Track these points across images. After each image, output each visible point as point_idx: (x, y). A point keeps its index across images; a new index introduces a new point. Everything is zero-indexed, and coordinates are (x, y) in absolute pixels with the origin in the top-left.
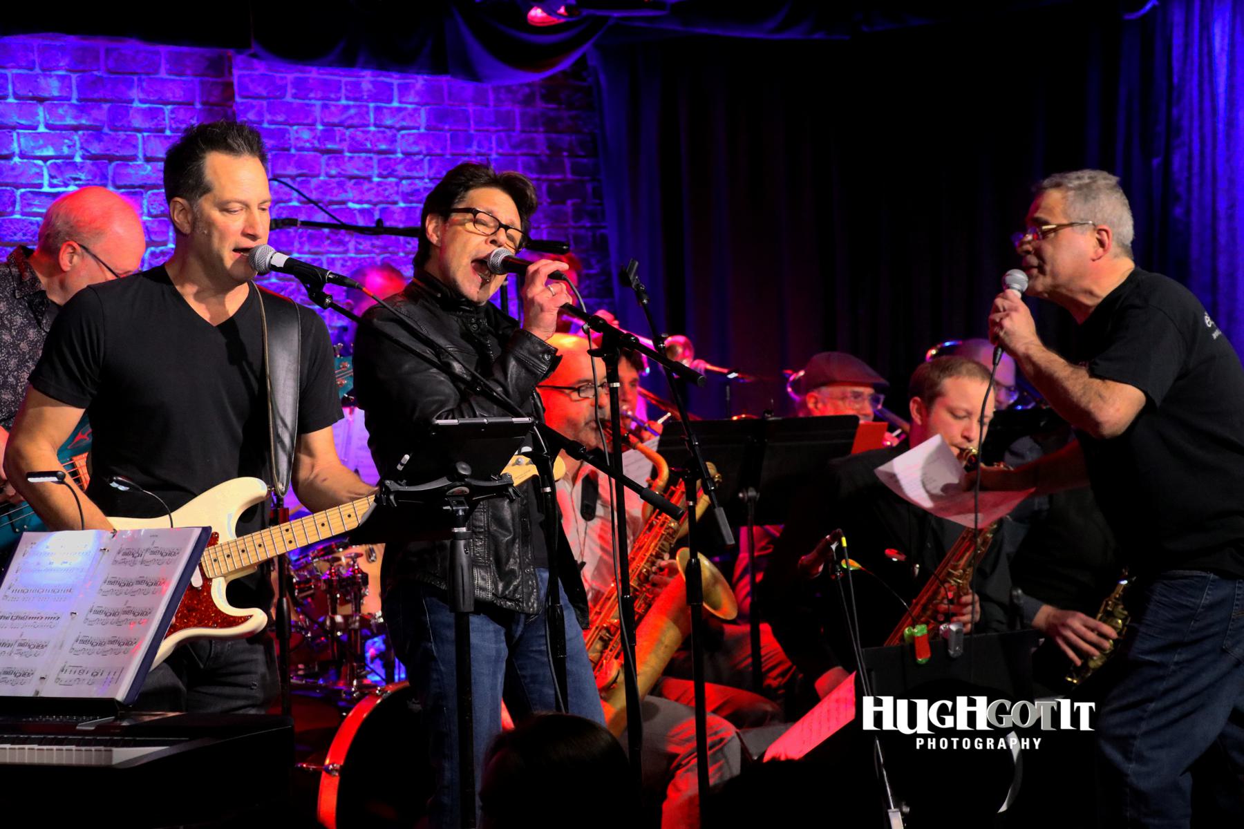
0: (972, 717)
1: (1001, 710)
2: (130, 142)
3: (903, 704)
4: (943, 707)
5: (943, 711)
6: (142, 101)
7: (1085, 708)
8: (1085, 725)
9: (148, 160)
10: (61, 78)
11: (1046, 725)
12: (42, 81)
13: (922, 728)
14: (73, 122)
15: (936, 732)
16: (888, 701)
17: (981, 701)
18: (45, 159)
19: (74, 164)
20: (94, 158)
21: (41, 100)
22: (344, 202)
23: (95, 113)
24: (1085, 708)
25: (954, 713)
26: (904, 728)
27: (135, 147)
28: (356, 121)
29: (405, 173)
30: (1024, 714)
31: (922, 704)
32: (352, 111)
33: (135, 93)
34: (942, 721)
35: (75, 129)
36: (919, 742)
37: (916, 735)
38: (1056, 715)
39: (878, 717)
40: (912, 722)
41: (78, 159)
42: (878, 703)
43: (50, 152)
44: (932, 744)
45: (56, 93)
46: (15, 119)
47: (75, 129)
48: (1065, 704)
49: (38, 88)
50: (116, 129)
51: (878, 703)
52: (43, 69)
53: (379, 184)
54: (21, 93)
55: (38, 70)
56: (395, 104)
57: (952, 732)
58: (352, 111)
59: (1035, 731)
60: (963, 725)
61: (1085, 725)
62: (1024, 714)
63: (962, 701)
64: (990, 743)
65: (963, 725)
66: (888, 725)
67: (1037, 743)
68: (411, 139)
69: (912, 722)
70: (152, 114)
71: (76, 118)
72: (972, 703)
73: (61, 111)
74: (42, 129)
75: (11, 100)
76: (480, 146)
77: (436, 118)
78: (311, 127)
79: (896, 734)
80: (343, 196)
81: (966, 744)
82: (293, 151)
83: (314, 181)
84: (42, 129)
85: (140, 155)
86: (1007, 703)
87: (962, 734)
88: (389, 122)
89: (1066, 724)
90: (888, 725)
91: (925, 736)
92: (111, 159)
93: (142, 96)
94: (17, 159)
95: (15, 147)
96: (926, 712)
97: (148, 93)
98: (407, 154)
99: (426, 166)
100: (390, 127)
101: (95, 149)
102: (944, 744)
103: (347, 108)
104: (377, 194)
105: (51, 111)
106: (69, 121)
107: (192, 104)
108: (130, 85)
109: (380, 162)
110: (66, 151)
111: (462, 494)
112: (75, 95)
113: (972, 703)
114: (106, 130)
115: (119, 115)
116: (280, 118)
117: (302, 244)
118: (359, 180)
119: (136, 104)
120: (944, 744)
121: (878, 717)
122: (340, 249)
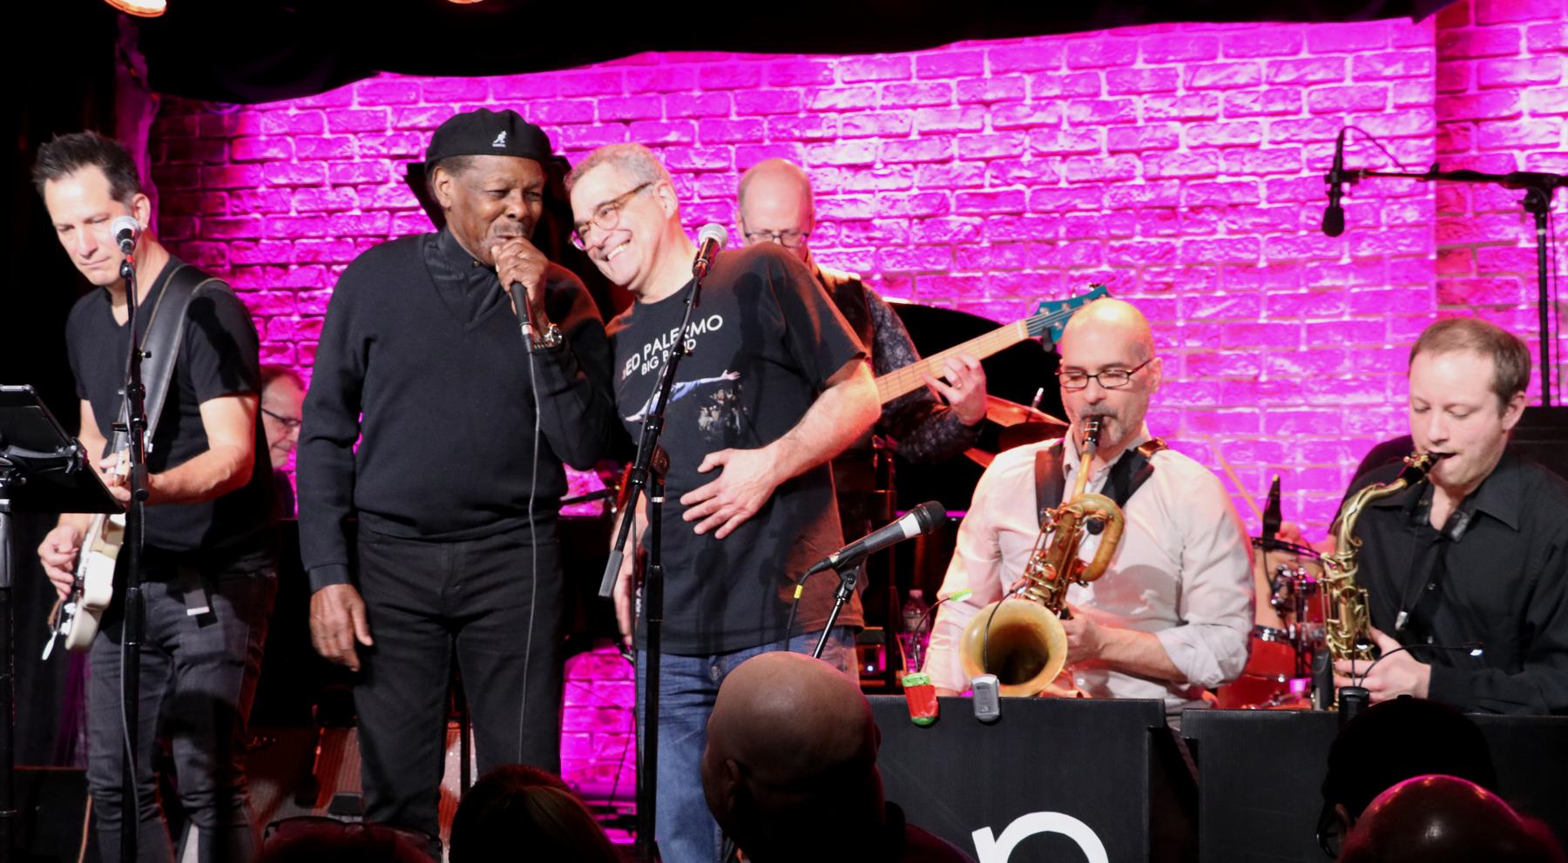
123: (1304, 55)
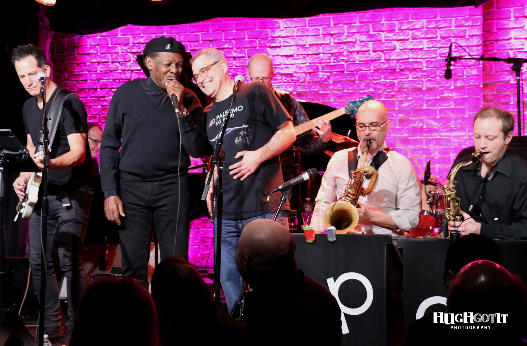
0: (468, 319)
1: (478, 317)
3: (446, 315)
5: (459, 317)
7: (505, 316)
8: (505, 322)
11: (492, 322)
13: (452, 322)
15: (457, 324)
17: (471, 314)
24: (505, 316)
25: (463, 318)
26: (446, 322)
30: (485, 318)
31: (452, 315)
34: (459, 320)
36: (452, 327)
37: (450, 325)
38: (495, 319)
39: (438, 319)
40: (449, 321)
42: (438, 314)
44: (455, 328)
48: (498, 315)
51: (438, 314)
57: (462, 324)
59: (489, 323)
60: (465, 321)
61: (505, 322)
62: (485, 318)
63: (465, 314)
64: (474, 327)
65: (465, 321)
66: (441, 321)
69: (449, 321)
72: (468, 314)
86: (480, 315)
87: (465, 324)
89: (499, 321)
90: (441, 321)
91: (453, 325)
94: (513, 40)
113: (468, 314)
121: (438, 319)
123: (438, 18)
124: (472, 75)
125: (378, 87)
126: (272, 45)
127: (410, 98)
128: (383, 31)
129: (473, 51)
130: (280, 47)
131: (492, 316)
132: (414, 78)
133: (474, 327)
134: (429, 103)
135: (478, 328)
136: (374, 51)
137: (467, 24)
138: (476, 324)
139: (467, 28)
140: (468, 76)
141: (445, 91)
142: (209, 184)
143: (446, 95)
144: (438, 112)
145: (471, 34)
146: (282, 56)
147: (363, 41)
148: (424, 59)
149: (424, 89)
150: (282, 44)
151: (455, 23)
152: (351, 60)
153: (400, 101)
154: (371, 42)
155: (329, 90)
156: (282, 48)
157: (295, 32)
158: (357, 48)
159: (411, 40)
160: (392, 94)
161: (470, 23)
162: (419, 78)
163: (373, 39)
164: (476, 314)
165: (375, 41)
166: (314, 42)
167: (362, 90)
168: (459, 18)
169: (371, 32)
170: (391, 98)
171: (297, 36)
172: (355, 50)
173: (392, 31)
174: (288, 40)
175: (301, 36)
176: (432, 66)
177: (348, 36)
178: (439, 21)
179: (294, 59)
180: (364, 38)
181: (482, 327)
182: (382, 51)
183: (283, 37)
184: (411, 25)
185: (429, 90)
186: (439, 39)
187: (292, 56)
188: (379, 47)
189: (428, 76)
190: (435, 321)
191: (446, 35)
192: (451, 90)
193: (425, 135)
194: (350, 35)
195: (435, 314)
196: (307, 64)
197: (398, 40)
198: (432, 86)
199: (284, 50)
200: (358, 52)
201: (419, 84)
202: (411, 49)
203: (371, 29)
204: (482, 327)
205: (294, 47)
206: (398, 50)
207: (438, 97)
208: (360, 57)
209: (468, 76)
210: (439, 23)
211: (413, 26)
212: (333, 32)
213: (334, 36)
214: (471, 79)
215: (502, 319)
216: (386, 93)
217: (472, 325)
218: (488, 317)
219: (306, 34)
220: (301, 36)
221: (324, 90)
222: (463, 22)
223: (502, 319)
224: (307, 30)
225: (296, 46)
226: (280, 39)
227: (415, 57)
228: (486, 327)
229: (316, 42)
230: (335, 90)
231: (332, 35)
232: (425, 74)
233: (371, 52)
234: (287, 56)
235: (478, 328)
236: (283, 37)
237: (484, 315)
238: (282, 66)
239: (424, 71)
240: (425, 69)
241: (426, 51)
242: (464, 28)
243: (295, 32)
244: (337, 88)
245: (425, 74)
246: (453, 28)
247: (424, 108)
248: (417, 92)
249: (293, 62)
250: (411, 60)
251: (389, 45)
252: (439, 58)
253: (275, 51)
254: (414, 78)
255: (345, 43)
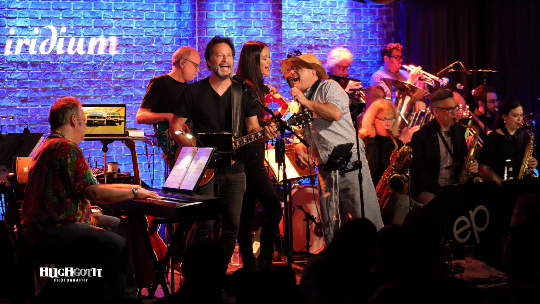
0: (69, 273)
1: (77, 271)
2: (249, 22)
3: (51, 270)
4: (62, 270)
5: (61, 271)
6: (254, 10)
7: (99, 271)
8: (99, 275)
9: (255, 27)
10: (230, 4)
11: (89, 275)
12: (225, 6)
13: (56, 276)
14: (233, 17)
15: (60, 277)
16: (47, 269)
17: (72, 269)
18: (224, 28)
19: (233, 29)
20: (238, 27)
21: (224, 11)
22: (319, 37)
23: (240, 14)
24: (99, 271)
25: (64, 272)
26: (51, 276)
27: (251, 24)
28: (324, 13)
29: (340, 28)
30: (83, 272)
31: (56, 270)
32: (323, 10)
33: (252, 8)
34: (61, 274)
35: (234, 19)
36: (55, 280)
37: (54, 278)
38: (92, 273)
39: (44, 273)
40: (53, 275)
41: (234, 28)
42: (44, 269)
43: (226, 25)
44: (58, 280)
45: (228, 9)
46: (216, 17)
47: (234, 19)
48: (94, 270)
49: (223, 8)
50: (246, 19)
51: (44, 269)
52: (225, 2)
53: (331, 32)
54: (218, 9)
55: (224, 2)
56: (337, 7)
57: (64, 277)
58: (323, 10)
59: (86, 277)
60: (67, 275)
61: (99, 275)
62: (83, 272)
63: (67, 269)
64: (74, 280)
65: (67, 275)
66: (47, 275)
67: (87, 280)
68: (342, 18)
69: (53, 275)
70: (257, 14)
71: (234, 16)
72: (69, 269)
73: (230, 14)
74: (224, 19)
75: (215, 11)
76: (364, 20)
77: (353, 11)
78: (310, 14)
79: (49, 277)
80: (319, 35)
81: (68, 280)
82: (304, 22)
83: (310, 31)
84: (224, 19)
85: (253, 26)
86: (79, 269)
87: (67, 278)
88: (335, 13)
89: (94, 275)
90: (47, 275)
91: (57, 278)
92: (244, 27)
93: (254, 9)
94: (216, 28)
95: (216, 25)
96: (57, 272)
97: (256, 8)
98: (341, 23)
99: (346, 26)
100: (335, 15)
101: (239, 25)
102: (62, 280)
103: (321, 9)
104: (330, 35)
105: (227, 14)
106: (232, 17)
107: (269, 11)
108: (250, 5)
109: (332, 25)
110: (230, 25)
111: (216, 155)
112: (234, 9)
113: (69, 269)
114: (243, 19)
115: (246, 16)
116: (301, 12)
117: (306, 50)
118: (324, 30)
119: (252, 11)
120: (62, 280)
121: (44, 273)
122: (318, 51)
123: (144, 2)
124: (168, 52)
125: (99, 59)
126: (9, 16)
127: (123, 70)
128: (103, 10)
129: (169, 32)
130: (15, 18)
131: (89, 270)
132: (126, 52)
133: (74, 280)
134: (138, 75)
135: (77, 280)
136: (95, 27)
137: (164, 9)
138: (76, 277)
139: (165, 13)
140: (165, 53)
141: (149, 65)
142: (237, 105)
143: (149, 68)
144: (144, 83)
145: (168, 18)
146: (18, 27)
147: (87, 18)
148: (134, 36)
149: (134, 62)
150: (17, 16)
151: (156, 7)
152: (78, 34)
153: (115, 72)
154: (93, 18)
155: (58, 61)
156: (17, 19)
157: (30, 5)
158: (82, 24)
159: (124, 19)
160: (109, 66)
161: (166, 9)
162: (130, 52)
163: (95, 16)
164: (76, 269)
165: (96, 18)
166: (46, 16)
167: (86, 61)
168: (160, 4)
169: (93, 10)
170: (108, 69)
171: (31, 9)
172: (81, 25)
173: (109, 10)
174: (24, 12)
175: (34, 9)
176: (140, 43)
177: (75, 12)
178: (145, 5)
179: (29, 30)
180: (88, 15)
181: (80, 280)
182: (102, 28)
183: (19, 9)
184: (125, 6)
185: (138, 63)
186: (144, 20)
187: (27, 27)
188: (100, 24)
189: (137, 51)
190: (41, 275)
191: (150, 17)
192: (153, 64)
193: (134, 102)
194: (76, 10)
195: (41, 269)
196: (40, 36)
197: (115, 19)
198: (140, 60)
199: (20, 22)
200: (83, 27)
201: (130, 58)
202: (124, 27)
203: (93, 7)
204: (80, 280)
205: (28, 19)
206: (114, 27)
207: (144, 70)
208: (85, 32)
209: (165, 53)
210: (145, 7)
211: (126, 7)
212: (62, 8)
213: (63, 11)
214: (168, 56)
215: (97, 273)
216: (104, 65)
217: (72, 278)
218: (85, 271)
219: (40, 8)
220: (34, 9)
221: (55, 61)
222: (162, 8)
223: (97, 273)
224: (40, 4)
225: (30, 18)
226: (16, 10)
227: (127, 34)
228: (84, 280)
229: (48, 16)
230: (63, 61)
231: (61, 10)
232: (135, 49)
233: (93, 28)
234: (22, 27)
235: (77, 280)
236: (19, 9)
237: (82, 270)
238: (18, 36)
239: (134, 47)
240: (134, 45)
241: (135, 30)
242: (163, 13)
243: (30, 5)
244: (65, 59)
245: (135, 49)
246: (154, 11)
247: (133, 79)
248: (128, 65)
249: (28, 33)
250: (124, 37)
251: (108, 23)
252: (144, 36)
253: (11, 22)
254: (126, 52)
255: (72, 18)
